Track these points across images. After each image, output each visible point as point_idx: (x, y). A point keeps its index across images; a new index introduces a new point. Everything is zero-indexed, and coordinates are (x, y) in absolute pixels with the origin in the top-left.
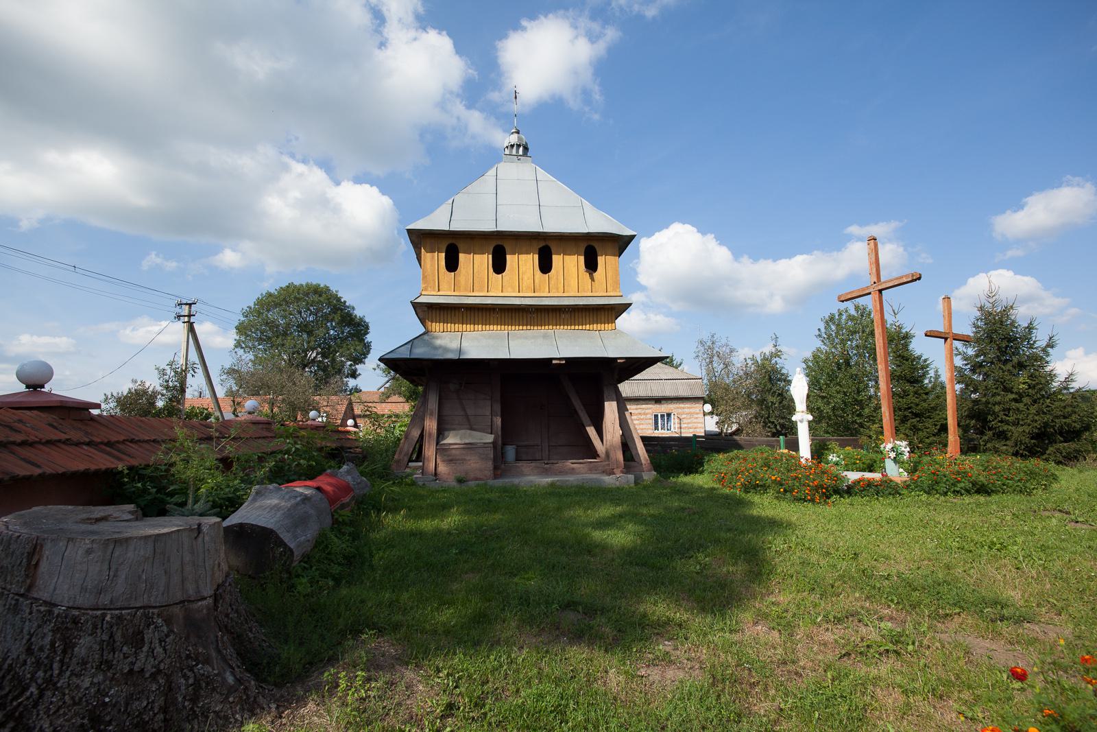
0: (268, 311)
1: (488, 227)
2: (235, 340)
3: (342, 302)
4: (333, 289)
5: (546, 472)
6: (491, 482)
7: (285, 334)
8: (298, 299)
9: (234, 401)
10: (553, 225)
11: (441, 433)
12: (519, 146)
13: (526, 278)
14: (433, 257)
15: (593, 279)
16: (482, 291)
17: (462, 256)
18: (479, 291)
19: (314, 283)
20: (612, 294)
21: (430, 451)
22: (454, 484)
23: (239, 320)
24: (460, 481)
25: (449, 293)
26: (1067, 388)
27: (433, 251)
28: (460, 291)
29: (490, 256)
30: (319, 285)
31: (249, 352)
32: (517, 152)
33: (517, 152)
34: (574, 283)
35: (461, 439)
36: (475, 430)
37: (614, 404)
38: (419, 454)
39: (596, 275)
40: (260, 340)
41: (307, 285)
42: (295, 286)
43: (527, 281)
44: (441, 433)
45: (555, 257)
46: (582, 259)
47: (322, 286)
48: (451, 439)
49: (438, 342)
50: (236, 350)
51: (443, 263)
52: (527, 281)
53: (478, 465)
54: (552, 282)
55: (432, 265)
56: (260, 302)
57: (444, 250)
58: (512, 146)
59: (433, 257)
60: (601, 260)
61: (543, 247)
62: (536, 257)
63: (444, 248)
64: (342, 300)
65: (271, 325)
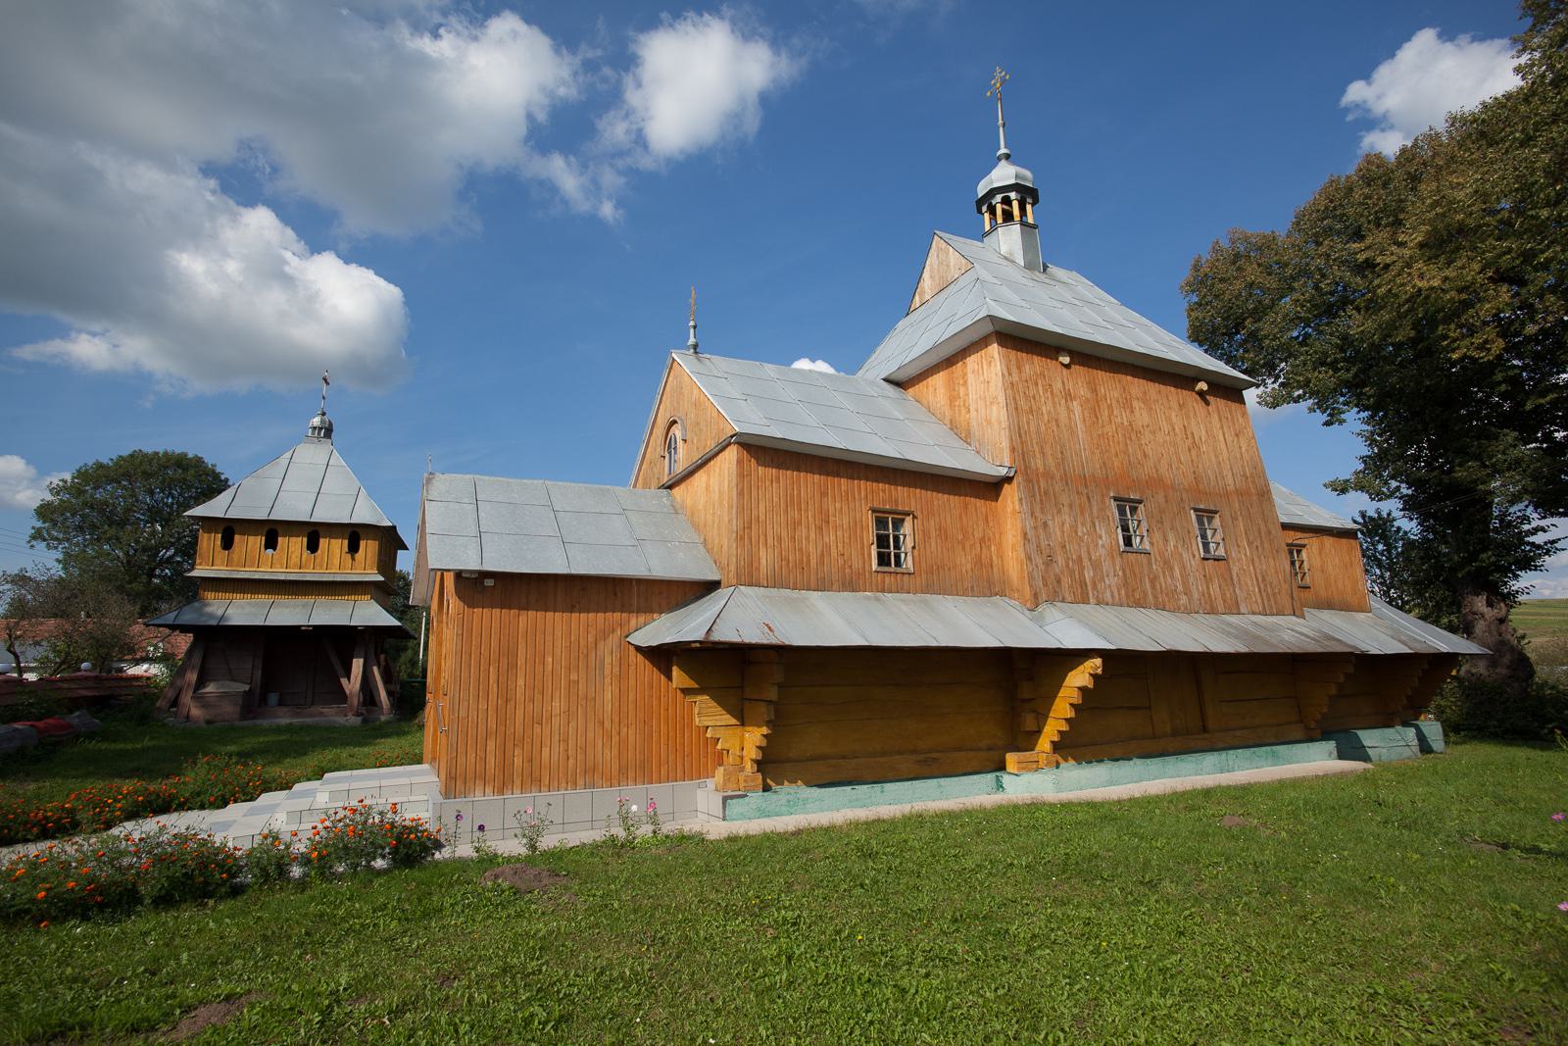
0: (96, 488)
1: (262, 515)
2: (33, 528)
3: (222, 481)
4: (209, 460)
5: (298, 715)
6: (238, 723)
7: (122, 524)
8: (147, 475)
9: (10, 636)
10: (322, 515)
11: (201, 682)
12: (321, 429)
13: (294, 557)
14: (209, 538)
15: (353, 559)
16: (253, 567)
17: (237, 537)
18: (249, 567)
19: (178, 451)
20: (369, 572)
21: (187, 699)
22: (204, 725)
23: (42, 500)
24: (209, 722)
25: (222, 568)
26: (1515, 597)
27: (210, 532)
28: (231, 566)
29: (264, 538)
30: (186, 455)
31: (56, 548)
32: (319, 434)
33: (319, 434)
34: (336, 562)
35: (218, 688)
36: (235, 681)
37: (361, 660)
38: (175, 703)
39: (357, 556)
40: (80, 529)
41: (166, 453)
42: (145, 455)
43: (295, 558)
44: (201, 682)
45: (322, 541)
46: (346, 542)
47: (190, 456)
48: (210, 688)
49: (209, 609)
50: (34, 543)
51: (219, 543)
52: (295, 558)
53: (230, 709)
54: (318, 561)
55: (209, 544)
56: (83, 475)
57: (221, 531)
58: (315, 428)
59: (209, 538)
60: (362, 543)
61: (313, 531)
62: (305, 540)
63: (221, 530)
64: (223, 477)
65: (100, 507)
